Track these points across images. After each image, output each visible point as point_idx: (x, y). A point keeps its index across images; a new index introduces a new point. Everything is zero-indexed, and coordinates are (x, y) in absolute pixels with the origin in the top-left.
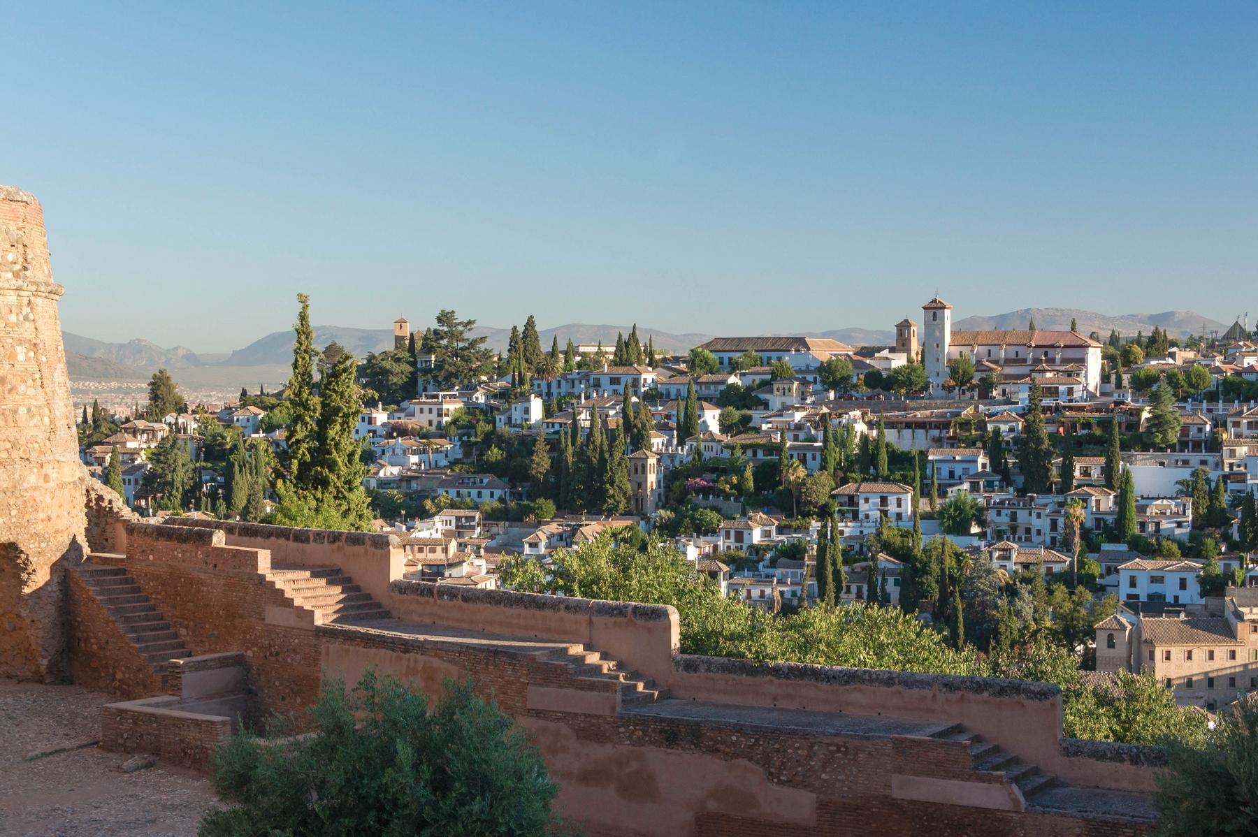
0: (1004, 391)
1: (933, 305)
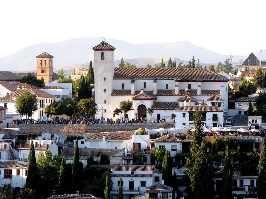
0: (158, 116)
1: (104, 47)
